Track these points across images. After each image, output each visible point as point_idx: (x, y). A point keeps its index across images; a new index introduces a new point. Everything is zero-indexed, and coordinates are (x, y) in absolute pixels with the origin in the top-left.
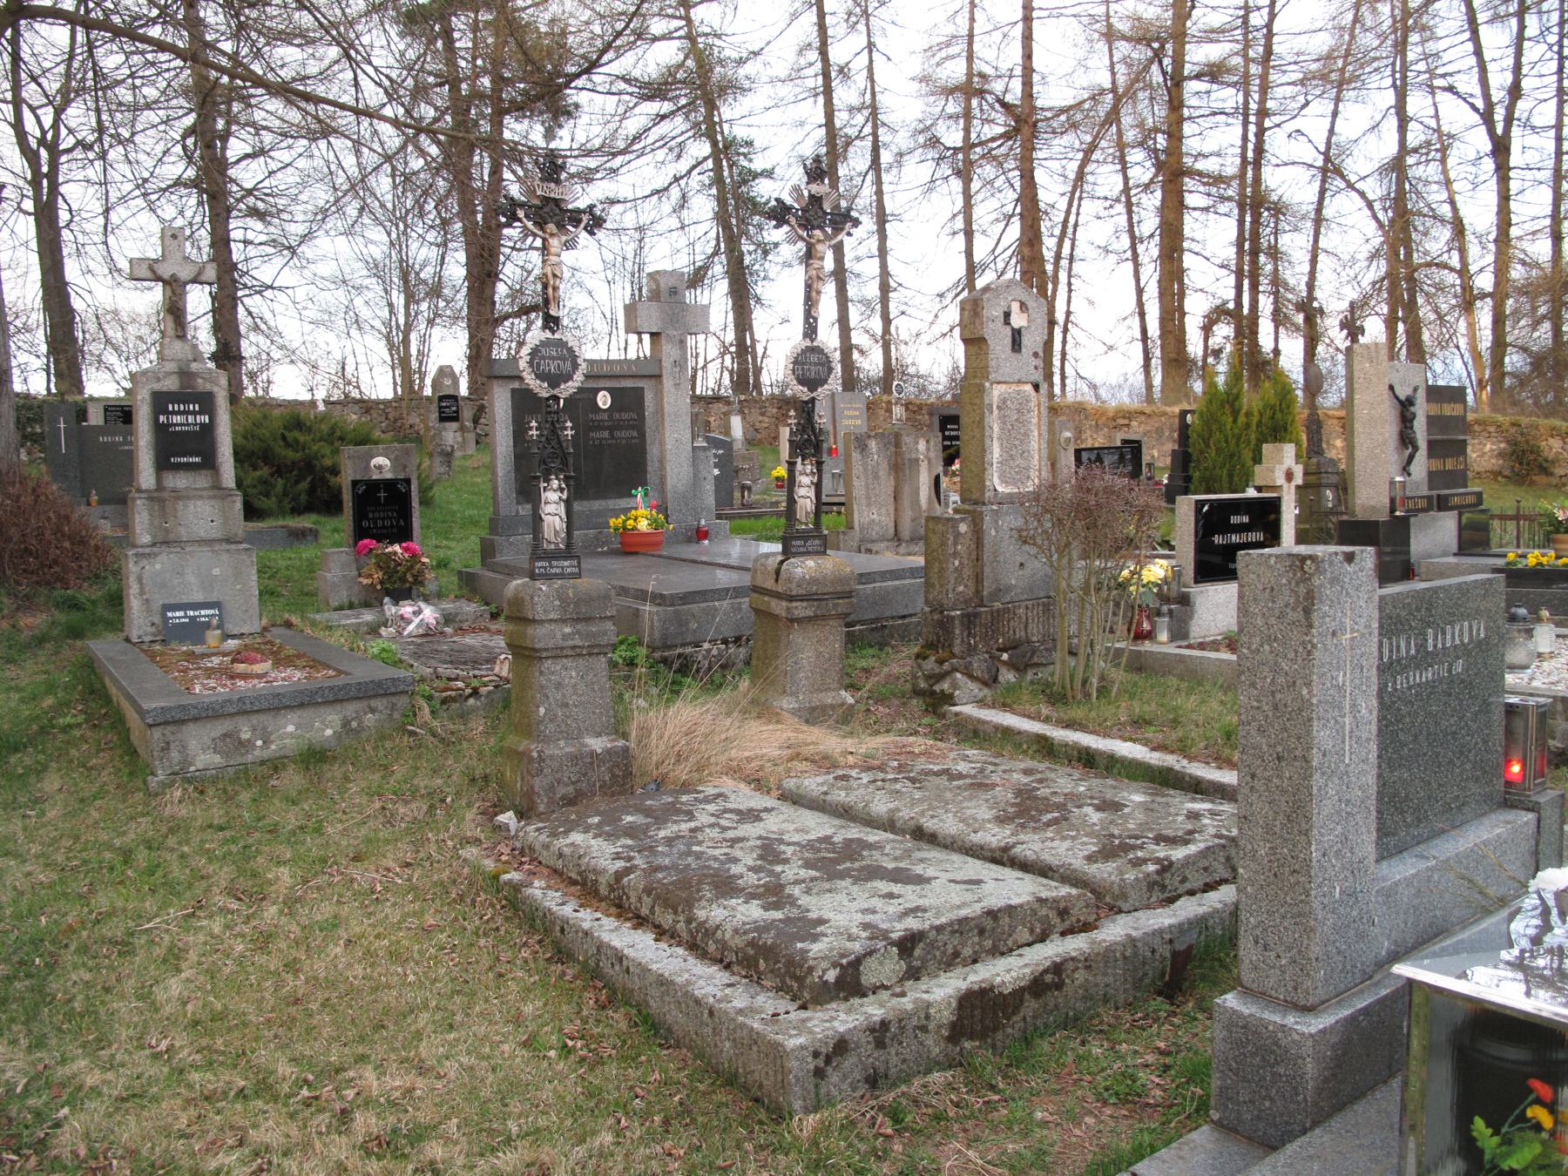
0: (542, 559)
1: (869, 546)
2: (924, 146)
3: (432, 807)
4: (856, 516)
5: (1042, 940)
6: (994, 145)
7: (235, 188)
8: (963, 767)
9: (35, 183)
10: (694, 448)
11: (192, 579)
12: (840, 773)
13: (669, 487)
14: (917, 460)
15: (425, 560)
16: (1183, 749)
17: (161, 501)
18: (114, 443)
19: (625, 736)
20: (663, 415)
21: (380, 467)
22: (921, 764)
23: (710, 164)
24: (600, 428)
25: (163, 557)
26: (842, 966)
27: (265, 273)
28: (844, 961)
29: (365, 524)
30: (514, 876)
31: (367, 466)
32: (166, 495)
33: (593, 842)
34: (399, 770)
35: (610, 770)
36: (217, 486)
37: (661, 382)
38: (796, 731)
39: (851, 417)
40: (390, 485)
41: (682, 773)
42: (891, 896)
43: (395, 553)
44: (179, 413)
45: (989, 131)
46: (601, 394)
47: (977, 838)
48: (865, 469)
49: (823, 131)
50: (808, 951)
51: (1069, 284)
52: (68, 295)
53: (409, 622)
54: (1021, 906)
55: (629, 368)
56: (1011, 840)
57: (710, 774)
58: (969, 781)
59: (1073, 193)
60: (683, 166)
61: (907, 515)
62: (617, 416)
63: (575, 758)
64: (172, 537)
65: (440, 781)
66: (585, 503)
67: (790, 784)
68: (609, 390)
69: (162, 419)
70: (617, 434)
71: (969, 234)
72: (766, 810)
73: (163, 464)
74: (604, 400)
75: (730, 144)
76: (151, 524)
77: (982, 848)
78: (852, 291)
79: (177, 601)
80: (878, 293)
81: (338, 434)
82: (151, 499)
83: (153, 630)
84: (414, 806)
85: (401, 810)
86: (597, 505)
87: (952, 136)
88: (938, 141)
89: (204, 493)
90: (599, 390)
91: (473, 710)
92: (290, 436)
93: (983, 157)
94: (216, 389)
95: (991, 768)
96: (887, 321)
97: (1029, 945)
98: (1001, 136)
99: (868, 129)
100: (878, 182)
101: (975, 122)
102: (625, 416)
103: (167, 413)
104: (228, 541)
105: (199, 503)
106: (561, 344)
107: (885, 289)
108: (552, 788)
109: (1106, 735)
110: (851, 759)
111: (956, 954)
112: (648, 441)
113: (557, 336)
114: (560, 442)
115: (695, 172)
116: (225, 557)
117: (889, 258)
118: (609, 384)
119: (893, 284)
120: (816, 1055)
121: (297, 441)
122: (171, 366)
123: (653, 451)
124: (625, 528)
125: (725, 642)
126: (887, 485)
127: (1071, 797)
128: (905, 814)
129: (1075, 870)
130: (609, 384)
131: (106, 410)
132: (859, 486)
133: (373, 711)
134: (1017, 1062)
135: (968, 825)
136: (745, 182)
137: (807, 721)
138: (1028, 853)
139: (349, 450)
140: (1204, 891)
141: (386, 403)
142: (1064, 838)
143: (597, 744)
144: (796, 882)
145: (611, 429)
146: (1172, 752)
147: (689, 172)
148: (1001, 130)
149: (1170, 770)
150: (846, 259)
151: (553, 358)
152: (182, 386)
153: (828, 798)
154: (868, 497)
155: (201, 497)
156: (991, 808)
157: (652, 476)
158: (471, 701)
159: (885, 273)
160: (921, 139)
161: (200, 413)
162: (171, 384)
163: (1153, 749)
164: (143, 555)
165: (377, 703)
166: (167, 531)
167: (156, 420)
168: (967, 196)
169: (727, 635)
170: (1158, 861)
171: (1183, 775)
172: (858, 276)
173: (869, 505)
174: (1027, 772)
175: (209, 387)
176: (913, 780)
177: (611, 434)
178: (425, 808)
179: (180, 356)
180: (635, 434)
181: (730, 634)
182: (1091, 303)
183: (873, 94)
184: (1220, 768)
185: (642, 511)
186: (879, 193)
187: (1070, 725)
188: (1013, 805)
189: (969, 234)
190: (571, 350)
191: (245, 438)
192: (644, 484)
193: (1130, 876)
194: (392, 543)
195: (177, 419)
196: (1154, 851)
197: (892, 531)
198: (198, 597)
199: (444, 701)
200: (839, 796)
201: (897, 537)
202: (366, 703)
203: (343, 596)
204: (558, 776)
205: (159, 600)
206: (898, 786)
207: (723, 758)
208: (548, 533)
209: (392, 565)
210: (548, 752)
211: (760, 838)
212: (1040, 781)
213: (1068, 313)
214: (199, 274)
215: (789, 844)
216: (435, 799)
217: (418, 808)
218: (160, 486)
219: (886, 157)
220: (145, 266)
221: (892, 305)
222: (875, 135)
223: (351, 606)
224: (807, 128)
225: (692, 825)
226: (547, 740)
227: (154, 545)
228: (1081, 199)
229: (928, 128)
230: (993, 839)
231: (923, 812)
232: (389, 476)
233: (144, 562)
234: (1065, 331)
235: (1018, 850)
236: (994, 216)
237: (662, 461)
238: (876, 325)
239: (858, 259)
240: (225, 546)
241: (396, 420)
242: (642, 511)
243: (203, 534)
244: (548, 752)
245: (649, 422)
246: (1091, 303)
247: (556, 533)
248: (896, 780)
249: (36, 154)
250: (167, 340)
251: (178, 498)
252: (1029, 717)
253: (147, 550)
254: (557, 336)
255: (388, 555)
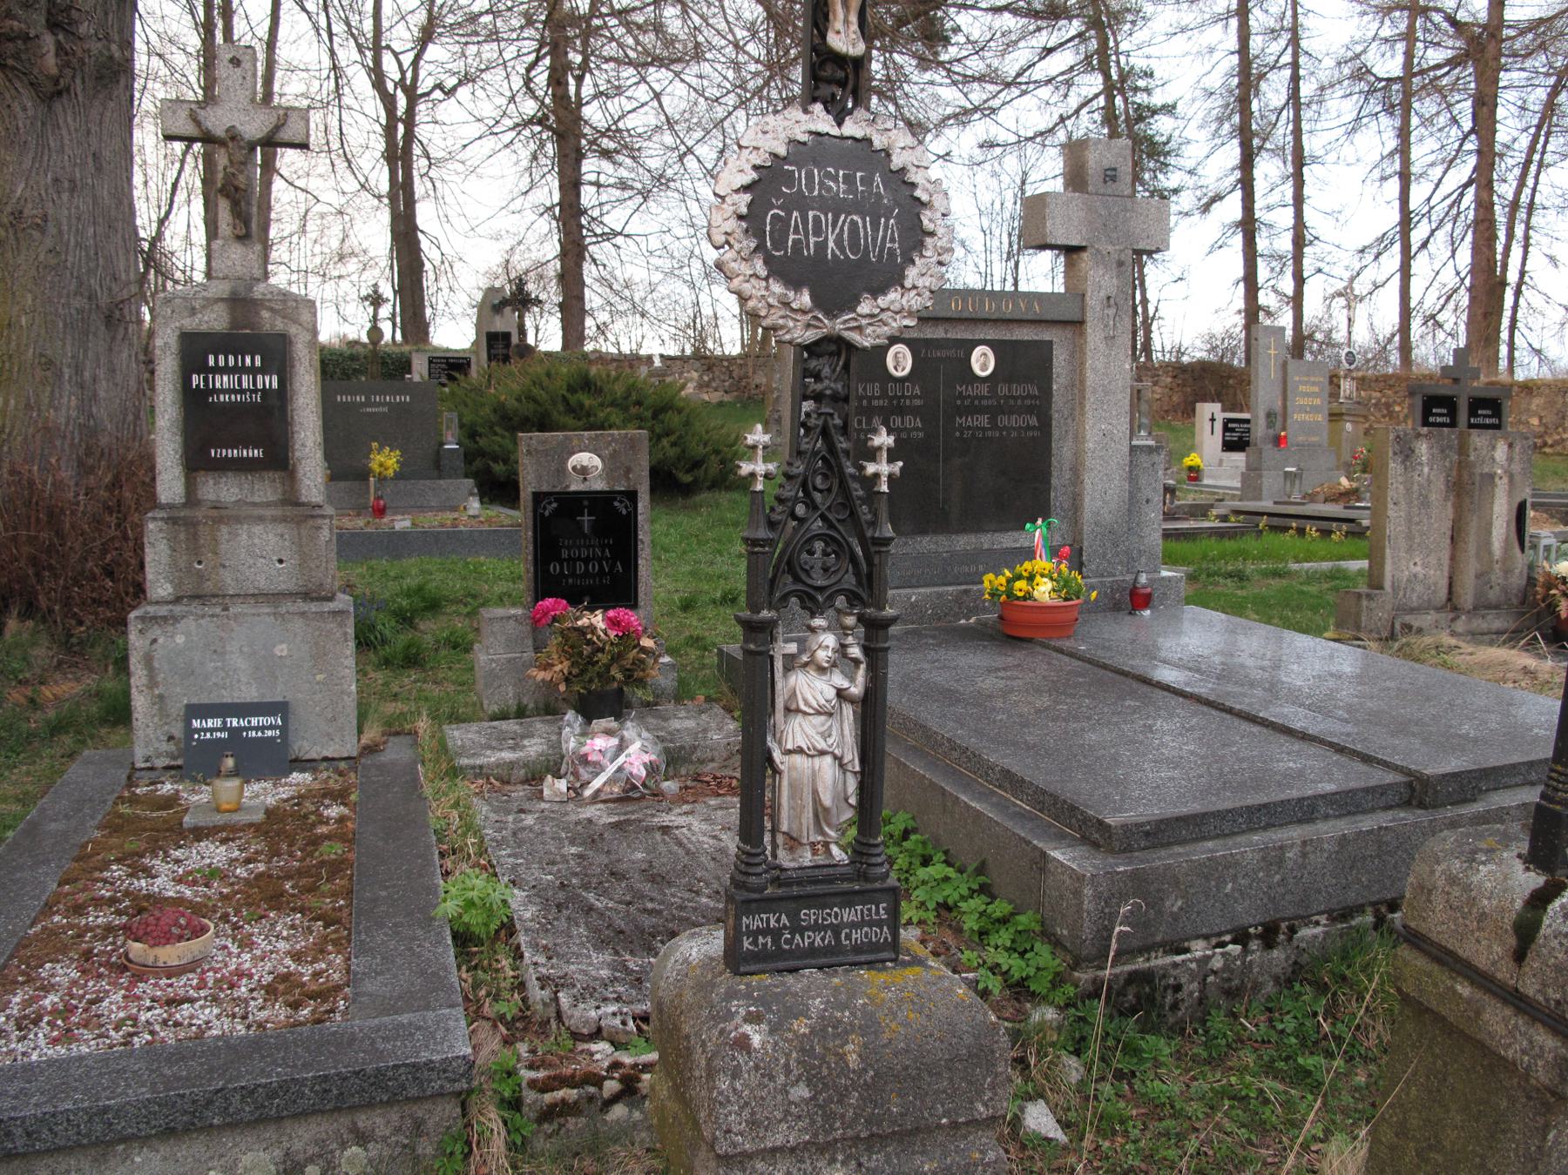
0: (768, 904)
1: (1408, 619)
2: (1352, 77)
4: (1388, 568)
6: (1439, 73)
7: (587, 130)
9: (389, 131)
10: (1133, 449)
11: (239, 662)
13: (1087, 515)
14: (1492, 476)
15: (647, 642)
17: (191, 525)
18: (354, 403)
20: (1082, 391)
21: (583, 471)
23: (1101, 101)
24: (973, 410)
25: (189, 623)
27: (614, 220)
29: (554, 568)
31: (561, 470)
32: (199, 514)
36: (291, 499)
37: (1082, 334)
39: (1308, 395)
40: (600, 502)
43: (592, 628)
44: (226, 370)
45: (1435, 56)
46: (978, 351)
48: (1408, 490)
49: (1235, 59)
51: (1527, 238)
52: (418, 242)
53: (598, 768)
55: (1029, 307)
59: (1539, 127)
60: (1073, 102)
61: (1470, 568)
62: (1003, 389)
64: (209, 587)
66: (942, 539)
68: (994, 345)
69: (196, 380)
70: (1003, 421)
71: (1405, 177)
73: (196, 461)
74: (982, 362)
75: (1124, 76)
76: (174, 563)
78: (1262, 244)
79: (213, 698)
80: (1289, 247)
81: (634, 397)
82: (173, 521)
83: (172, 747)
86: (964, 542)
87: (1389, 65)
88: (1369, 72)
89: (269, 512)
90: (976, 343)
91: (624, 1133)
92: (573, 399)
93: (1424, 87)
94: (293, 330)
96: (1299, 280)
98: (1449, 62)
99: (1287, 58)
100: (1297, 120)
101: (1420, 45)
102: (1017, 390)
103: (205, 369)
104: (307, 596)
105: (258, 529)
106: (866, 154)
107: (1299, 242)
112: (1056, 433)
113: (851, 128)
114: (847, 503)
115: (1084, 111)
116: (298, 625)
117: (1305, 207)
118: (992, 333)
119: (1308, 237)
121: (581, 406)
122: (221, 289)
123: (1062, 451)
124: (1010, 593)
125: (1241, 938)
126: (1441, 517)
130: (992, 333)
131: (430, 362)
132: (1395, 517)
133: (362, 1138)
136: (1140, 119)
139: (529, 440)
141: (731, 359)
145: (995, 412)
147: (1077, 112)
148: (1449, 54)
150: (1257, 206)
151: (837, 207)
152: (234, 323)
154: (1410, 537)
155: (261, 519)
157: (1058, 496)
158: (619, 1111)
159: (1299, 225)
160: (1346, 71)
161: (263, 370)
162: (215, 320)
164: (154, 619)
165: (377, 1121)
166: (200, 576)
167: (186, 381)
168: (1404, 134)
169: (1246, 920)
172: (1270, 226)
173: (1410, 550)
175: (279, 325)
177: (993, 420)
179: (240, 270)
180: (1034, 421)
181: (1250, 915)
182: (1553, 260)
183: (1295, 16)
185: (1042, 563)
186: (1297, 133)
189: (1405, 177)
190: (900, 180)
191: (518, 400)
192: (1046, 516)
194: (592, 610)
195: (222, 381)
197: (1443, 594)
198: (250, 694)
199: (549, 1114)
201: (1451, 603)
202: (345, 1120)
203: (508, 695)
205: (181, 697)
208: (791, 814)
209: (587, 650)
213: (1522, 273)
214: (278, 128)
218: (191, 499)
219: (1307, 89)
220: (183, 114)
221: (1306, 262)
222: (1295, 65)
223: (521, 713)
224: (1217, 56)
227: (177, 600)
228: (1548, 135)
229: (1358, 56)
232: (599, 486)
233: (156, 631)
234: (1518, 293)
236: (1432, 158)
237: (1076, 471)
238: (1287, 285)
239: (1269, 208)
240: (302, 606)
241: (741, 379)
242: (1042, 563)
243: (262, 583)
245: (1058, 401)
246: (1553, 260)
247: (821, 814)
249: (393, 97)
250: (219, 242)
251: (219, 521)
253: (164, 610)
254: (851, 128)
255: (582, 631)
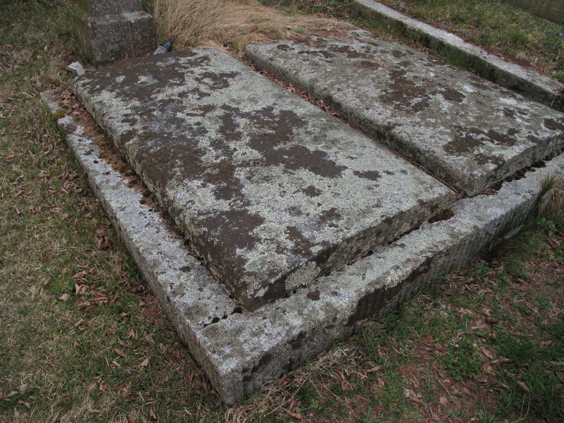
3: (35, 53)
5: (417, 228)
8: (356, 46)
12: (282, 43)
16: (484, 43)
19: (152, 11)
22: (331, 41)
26: (271, 285)
28: (273, 281)
30: (65, 121)
33: (115, 102)
34: (17, 26)
35: (141, 33)
38: (257, 10)
41: (186, 36)
42: (312, 192)
47: (369, 114)
50: (244, 261)
54: (409, 211)
56: (392, 120)
57: (203, 38)
58: (361, 59)
63: (117, 27)
65: (42, 34)
67: (250, 48)
72: (233, 75)
77: (371, 122)
84: (23, 52)
85: (15, 56)
95: (373, 48)
97: (408, 233)
108: (103, 46)
109: (438, 27)
110: (289, 33)
111: (359, 251)
120: (245, 370)
127: (429, 82)
128: (321, 85)
129: (437, 158)
134: (389, 330)
135: (362, 101)
137: (264, 4)
138: (404, 135)
140: (517, 178)
142: (427, 125)
143: (131, 17)
144: (245, 164)
146: (477, 45)
149: (476, 58)
153: (273, 63)
156: (377, 87)
163: (466, 41)
170: (496, 160)
171: (485, 63)
174: (397, 54)
176: (326, 54)
178: (30, 54)
184: (506, 61)
187: (417, 17)
188: (391, 86)
193: (478, 173)
196: (491, 150)
200: (280, 63)
204: (107, 38)
206: (316, 59)
207: (210, 28)
210: (98, 23)
211: (224, 107)
212: (406, 64)
215: (243, 116)
216: (36, 45)
217: (25, 54)
225: (182, 89)
226: (97, 14)
230: (380, 117)
231: (332, 85)
235: (396, 130)
244: (98, 23)
248: (315, 53)
252: (391, 7)
